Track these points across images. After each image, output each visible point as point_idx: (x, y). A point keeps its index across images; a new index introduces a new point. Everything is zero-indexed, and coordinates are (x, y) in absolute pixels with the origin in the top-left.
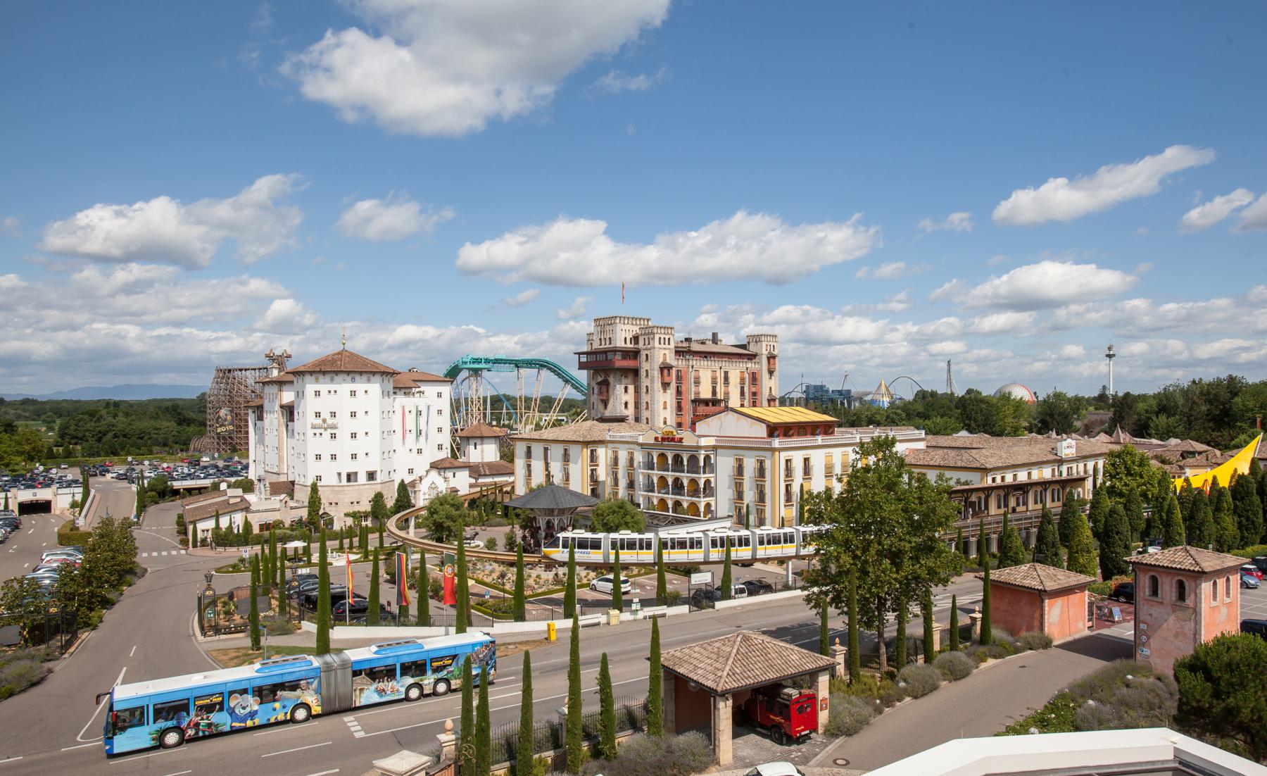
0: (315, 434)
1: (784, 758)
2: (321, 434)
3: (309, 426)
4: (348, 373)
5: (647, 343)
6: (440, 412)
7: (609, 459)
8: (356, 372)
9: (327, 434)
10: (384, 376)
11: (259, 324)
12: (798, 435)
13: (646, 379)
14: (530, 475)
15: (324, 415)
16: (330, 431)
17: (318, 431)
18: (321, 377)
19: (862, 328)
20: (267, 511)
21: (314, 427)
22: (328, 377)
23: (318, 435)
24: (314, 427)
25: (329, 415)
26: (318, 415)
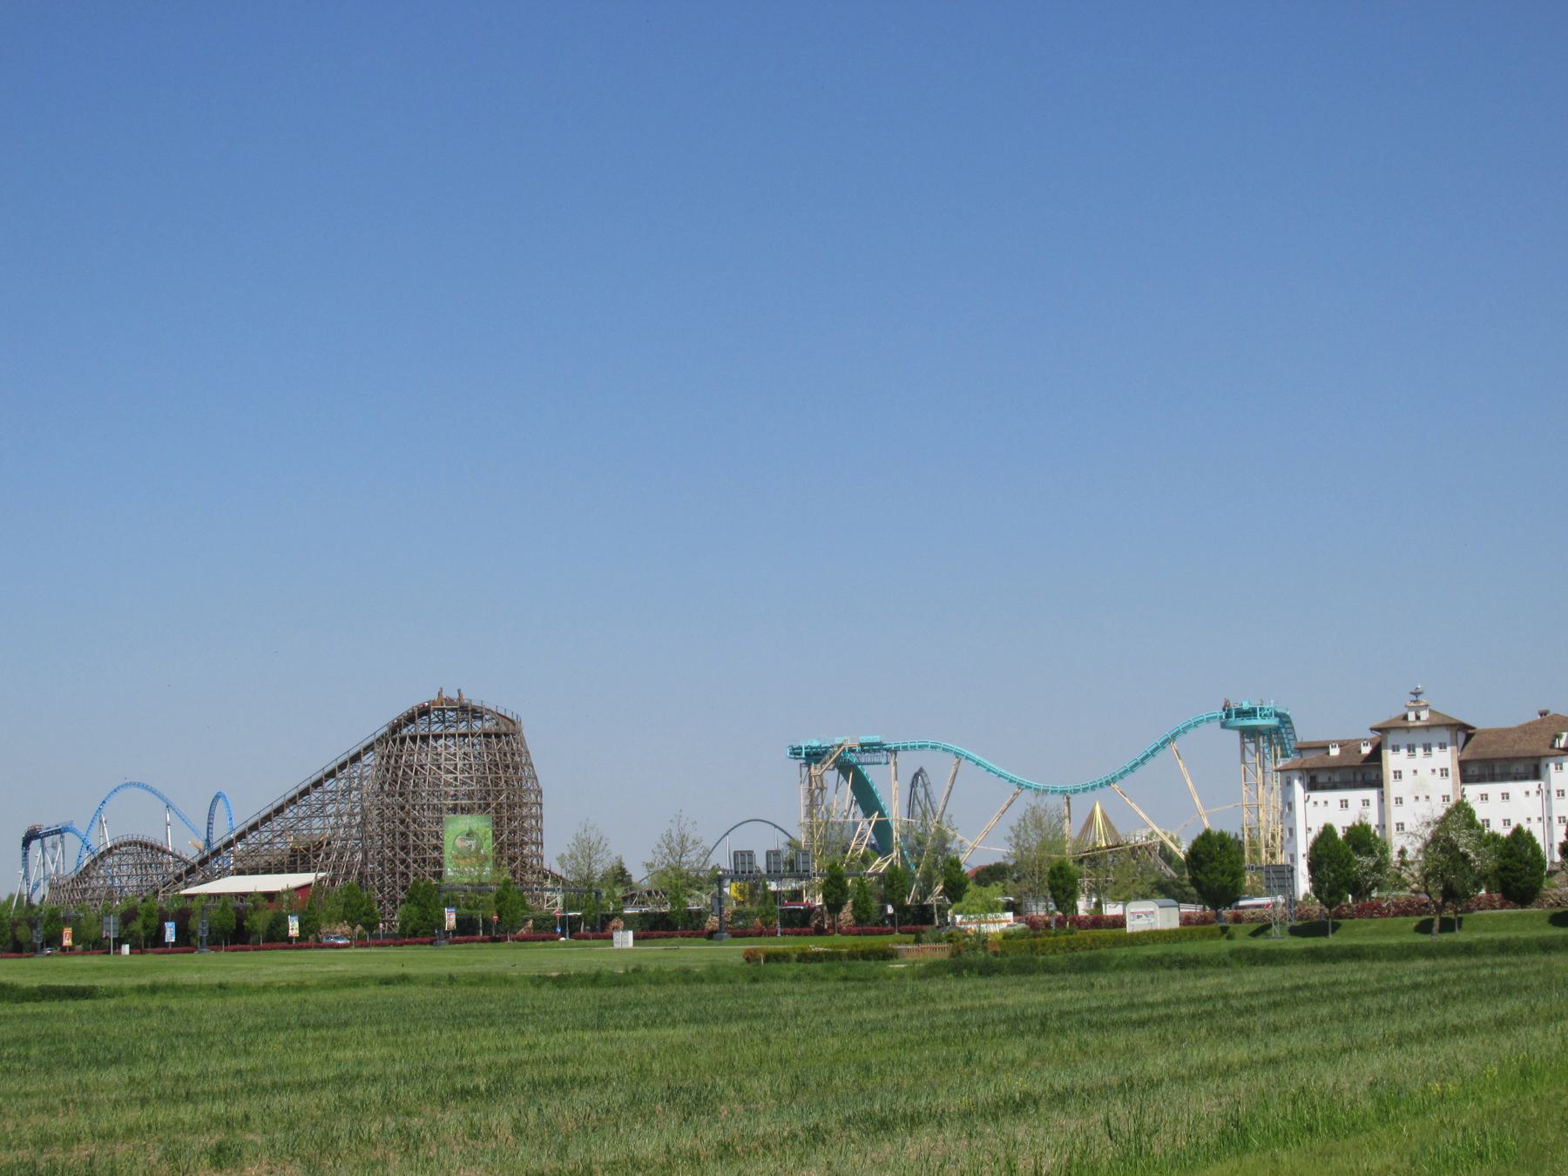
20: (386, 981)
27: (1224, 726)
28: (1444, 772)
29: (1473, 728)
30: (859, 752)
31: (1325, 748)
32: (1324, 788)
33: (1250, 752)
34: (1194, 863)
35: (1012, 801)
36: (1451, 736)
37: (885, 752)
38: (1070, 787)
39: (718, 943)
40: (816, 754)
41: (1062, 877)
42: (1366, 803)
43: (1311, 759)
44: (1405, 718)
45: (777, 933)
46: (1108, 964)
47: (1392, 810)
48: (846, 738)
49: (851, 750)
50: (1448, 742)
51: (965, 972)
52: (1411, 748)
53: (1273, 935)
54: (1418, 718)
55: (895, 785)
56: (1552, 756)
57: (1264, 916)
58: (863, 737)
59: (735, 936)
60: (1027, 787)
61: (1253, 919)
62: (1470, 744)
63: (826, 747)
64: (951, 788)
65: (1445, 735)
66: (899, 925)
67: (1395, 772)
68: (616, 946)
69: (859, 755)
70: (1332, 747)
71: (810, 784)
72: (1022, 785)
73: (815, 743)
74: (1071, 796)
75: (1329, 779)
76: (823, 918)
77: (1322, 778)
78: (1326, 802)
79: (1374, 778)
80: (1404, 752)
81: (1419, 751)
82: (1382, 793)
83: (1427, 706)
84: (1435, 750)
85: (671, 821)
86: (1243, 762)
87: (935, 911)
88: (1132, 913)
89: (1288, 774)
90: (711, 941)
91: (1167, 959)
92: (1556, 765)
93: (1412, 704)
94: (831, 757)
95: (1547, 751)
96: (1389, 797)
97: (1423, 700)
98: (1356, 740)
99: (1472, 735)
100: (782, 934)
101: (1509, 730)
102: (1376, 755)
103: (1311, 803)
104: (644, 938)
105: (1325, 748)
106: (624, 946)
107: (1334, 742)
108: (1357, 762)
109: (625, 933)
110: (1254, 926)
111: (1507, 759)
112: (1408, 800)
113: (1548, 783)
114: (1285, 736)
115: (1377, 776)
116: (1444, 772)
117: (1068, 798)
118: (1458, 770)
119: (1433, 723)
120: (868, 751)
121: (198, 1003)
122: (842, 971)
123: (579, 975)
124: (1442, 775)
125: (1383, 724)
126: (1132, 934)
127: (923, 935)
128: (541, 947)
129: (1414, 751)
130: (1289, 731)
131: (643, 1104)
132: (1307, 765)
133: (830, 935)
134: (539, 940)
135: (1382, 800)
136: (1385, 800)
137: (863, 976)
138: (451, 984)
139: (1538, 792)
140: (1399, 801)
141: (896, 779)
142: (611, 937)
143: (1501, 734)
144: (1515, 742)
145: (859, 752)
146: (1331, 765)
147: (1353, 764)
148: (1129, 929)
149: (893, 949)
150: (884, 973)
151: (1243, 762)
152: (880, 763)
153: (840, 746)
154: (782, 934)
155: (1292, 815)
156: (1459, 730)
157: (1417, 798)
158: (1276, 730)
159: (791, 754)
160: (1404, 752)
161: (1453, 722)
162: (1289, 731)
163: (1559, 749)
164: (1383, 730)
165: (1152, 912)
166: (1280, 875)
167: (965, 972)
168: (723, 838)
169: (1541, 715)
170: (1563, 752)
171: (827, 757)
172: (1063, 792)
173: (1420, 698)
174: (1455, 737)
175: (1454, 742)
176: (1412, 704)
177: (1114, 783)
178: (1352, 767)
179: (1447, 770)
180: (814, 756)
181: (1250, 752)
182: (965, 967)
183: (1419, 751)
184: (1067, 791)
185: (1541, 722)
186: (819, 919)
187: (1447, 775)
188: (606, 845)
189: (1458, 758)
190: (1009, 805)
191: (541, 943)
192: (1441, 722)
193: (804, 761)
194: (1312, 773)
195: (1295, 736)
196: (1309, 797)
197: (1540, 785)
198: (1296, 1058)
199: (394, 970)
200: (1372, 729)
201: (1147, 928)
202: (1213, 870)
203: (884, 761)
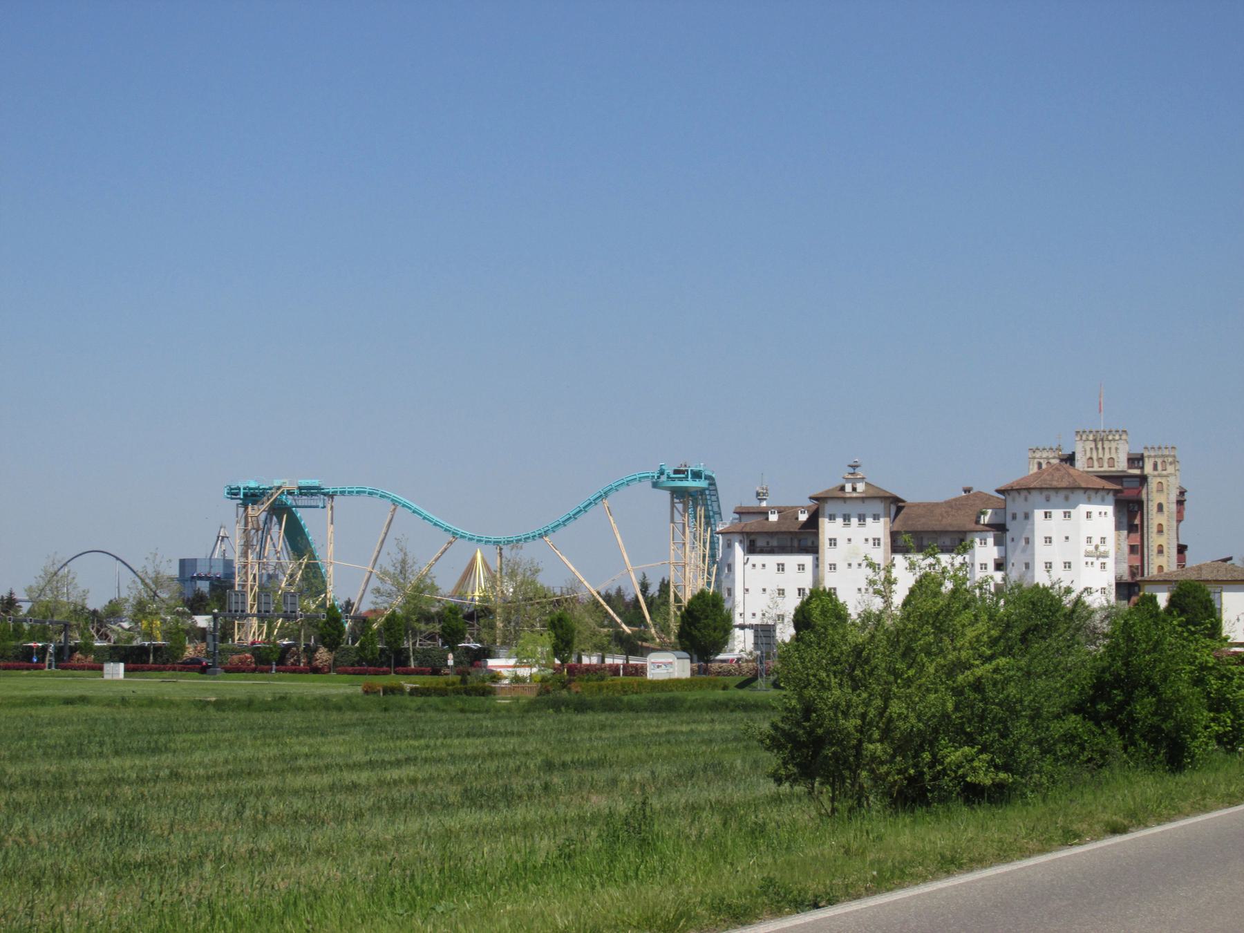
2: (1092, 563)
3: (1083, 553)
4: (1086, 489)
5: (1159, 467)
6: (1160, 508)
7: (498, 670)
9: (1097, 563)
12: (1158, 824)
13: (1159, 515)
17: (1090, 560)
18: (1092, 494)
19: (285, 643)
20: (68, 701)
21: (1088, 555)
24: (1088, 555)
27: (655, 485)
28: (877, 542)
29: (903, 501)
30: (298, 495)
31: (764, 513)
32: (762, 551)
33: (679, 511)
34: (690, 620)
35: (446, 549)
37: (322, 496)
38: (502, 538)
39: (212, 677)
40: (253, 495)
41: (562, 627)
42: (801, 567)
43: (752, 523)
44: (843, 488)
45: (271, 669)
46: (682, 706)
48: (285, 481)
49: (290, 493)
50: (882, 514)
51: (563, 709)
52: (847, 518)
53: (759, 688)
54: (854, 489)
55: (331, 528)
56: (977, 531)
57: (730, 670)
59: (227, 671)
60: (462, 537)
61: (720, 672)
62: (901, 516)
63: (264, 489)
64: (386, 534)
65: (879, 507)
66: (396, 666)
67: (830, 540)
68: (107, 677)
69: (296, 497)
70: (801, 512)
71: (246, 524)
72: (457, 534)
73: (253, 484)
74: (504, 547)
75: (768, 543)
76: (299, 657)
77: (761, 542)
78: (764, 565)
79: (809, 544)
81: (854, 521)
82: (817, 559)
83: (863, 478)
84: (869, 520)
85: (147, 559)
86: (672, 521)
87: (411, 654)
88: (653, 663)
89: (729, 537)
90: (204, 676)
91: (732, 703)
92: (981, 540)
93: (850, 477)
94: (268, 500)
95: (972, 526)
96: (823, 563)
97: (860, 473)
98: (792, 508)
99: (902, 508)
100: (277, 671)
101: (937, 505)
102: (813, 522)
103: (749, 565)
104: (134, 670)
105: (764, 513)
106: (115, 678)
107: (773, 508)
108: (795, 528)
109: (116, 665)
110: (740, 679)
111: (935, 532)
112: (842, 566)
113: (973, 556)
114: (708, 497)
115: (813, 543)
116: (877, 542)
117: (501, 549)
118: (889, 540)
119: (868, 496)
120: (305, 495)
122: (459, 704)
123: (233, 701)
124: (874, 545)
125: (822, 493)
126: (651, 682)
127: (468, 677)
128: (27, 676)
129: (864, 521)
130: (712, 493)
131: (694, 779)
132: (747, 529)
133: (325, 673)
134: (22, 669)
135: (816, 565)
136: (820, 566)
137: (476, 709)
138: (124, 705)
140: (833, 567)
141: (332, 523)
142: (101, 669)
143: (930, 507)
144: (943, 517)
145: (298, 495)
146: (770, 531)
147: (792, 530)
148: (649, 677)
149: (491, 687)
150: (494, 706)
151: (672, 521)
152: (317, 507)
153: (279, 488)
154: (277, 671)
155: (731, 576)
156: (892, 503)
157: (850, 565)
158: (702, 491)
159: (228, 493)
160: (840, 521)
161: (888, 495)
162: (712, 493)
163: (984, 525)
164: (819, 499)
165: (671, 663)
166: (767, 634)
167: (563, 709)
168: (62, 567)
169: (965, 492)
170: (987, 528)
171: (265, 498)
172: (497, 543)
173: (857, 470)
175: (887, 515)
176: (850, 477)
177: (546, 535)
178: (791, 533)
179: (879, 539)
180: (252, 497)
181: (679, 511)
182: (563, 704)
183: (854, 521)
184: (500, 542)
185: (967, 498)
186: (295, 658)
187: (879, 544)
188: (74, 578)
189: (890, 528)
190: (443, 553)
191: (25, 672)
192: (876, 495)
193: (241, 502)
194: (752, 537)
195: (718, 498)
196: (748, 559)
198: (797, 796)
200: (811, 498)
201: (666, 677)
202: (707, 626)
203: (321, 505)
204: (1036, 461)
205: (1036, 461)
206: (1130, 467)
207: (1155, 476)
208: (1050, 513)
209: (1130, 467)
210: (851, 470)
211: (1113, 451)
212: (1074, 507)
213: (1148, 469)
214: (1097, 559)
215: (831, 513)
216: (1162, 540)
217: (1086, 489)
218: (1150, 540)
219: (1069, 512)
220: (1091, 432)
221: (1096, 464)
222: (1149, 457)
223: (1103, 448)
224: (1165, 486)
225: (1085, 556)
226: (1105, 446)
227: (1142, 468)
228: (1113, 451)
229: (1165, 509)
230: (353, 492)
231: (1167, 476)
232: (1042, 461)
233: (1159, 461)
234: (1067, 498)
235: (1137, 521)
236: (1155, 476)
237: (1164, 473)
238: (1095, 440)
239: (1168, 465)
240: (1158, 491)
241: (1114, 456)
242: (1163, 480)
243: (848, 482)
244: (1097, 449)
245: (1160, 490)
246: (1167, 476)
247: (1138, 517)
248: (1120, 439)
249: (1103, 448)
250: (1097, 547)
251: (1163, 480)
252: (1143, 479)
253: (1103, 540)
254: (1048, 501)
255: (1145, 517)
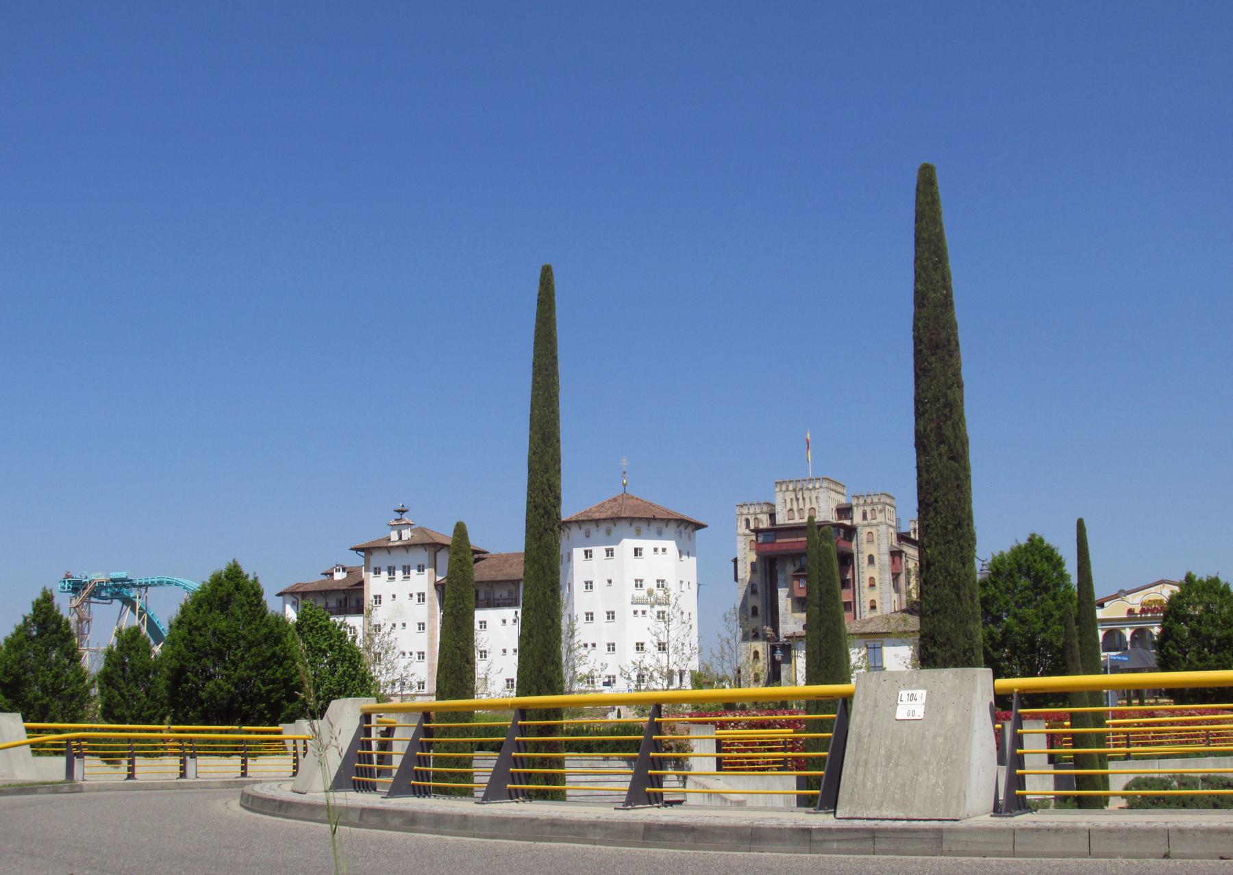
0: (635, 612)
1: (917, 596)
2: (644, 612)
4: (631, 520)
5: (869, 516)
6: (871, 560)
8: (640, 519)
10: (682, 528)
11: (1040, 586)
13: (871, 568)
14: (299, 793)
15: (650, 583)
16: (658, 608)
17: (640, 608)
18: (643, 526)
21: (635, 602)
22: (654, 527)
23: (640, 613)
24: (635, 602)
25: (656, 583)
26: (639, 583)
36: (429, 556)
47: (427, 648)
50: (426, 563)
52: (391, 571)
58: (113, 574)
65: (423, 556)
80: (384, 574)
81: (399, 574)
121: (268, 811)
124: (419, 600)
139: (515, 621)
160: (384, 574)
174: (433, 558)
176: (396, 523)
183: (399, 574)
197: (516, 613)
199: (850, 821)
204: (744, 517)
205: (744, 517)
206: (840, 518)
207: (864, 526)
208: (591, 551)
209: (840, 518)
210: (398, 516)
211: (814, 500)
212: (617, 542)
213: (857, 518)
214: (652, 606)
215: (376, 566)
216: (874, 595)
217: (631, 520)
218: (862, 595)
219: (612, 550)
220: (868, 496)
221: (796, 515)
222: (858, 505)
223: (804, 499)
224: (875, 537)
225: (632, 603)
226: (805, 496)
227: (852, 519)
228: (814, 500)
229: (876, 561)
230: (163, 582)
231: (877, 525)
232: (749, 517)
233: (868, 509)
234: (609, 532)
235: (849, 576)
236: (864, 526)
237: (874, 522)
238: (794, 490)
239: (877, 513)
240: (868, 542)
241: (814, 505)
242: (874, 530)
243: (393, 530)
244: (797, 499)
245: (870, 541)
246: (877, 525)
247: (850, 572)
248: (821, 487)
249: (804, 499)
250: (650, 593)
251: (874, 530)
252: (851, 532)
253: (661, 583)
254: (587, 536)
255: (856, 571)
